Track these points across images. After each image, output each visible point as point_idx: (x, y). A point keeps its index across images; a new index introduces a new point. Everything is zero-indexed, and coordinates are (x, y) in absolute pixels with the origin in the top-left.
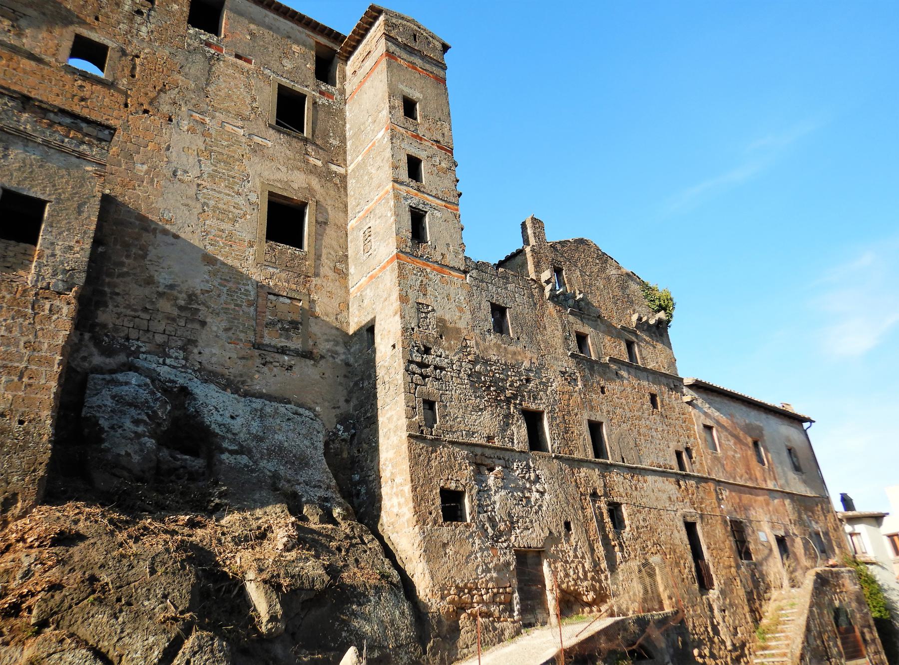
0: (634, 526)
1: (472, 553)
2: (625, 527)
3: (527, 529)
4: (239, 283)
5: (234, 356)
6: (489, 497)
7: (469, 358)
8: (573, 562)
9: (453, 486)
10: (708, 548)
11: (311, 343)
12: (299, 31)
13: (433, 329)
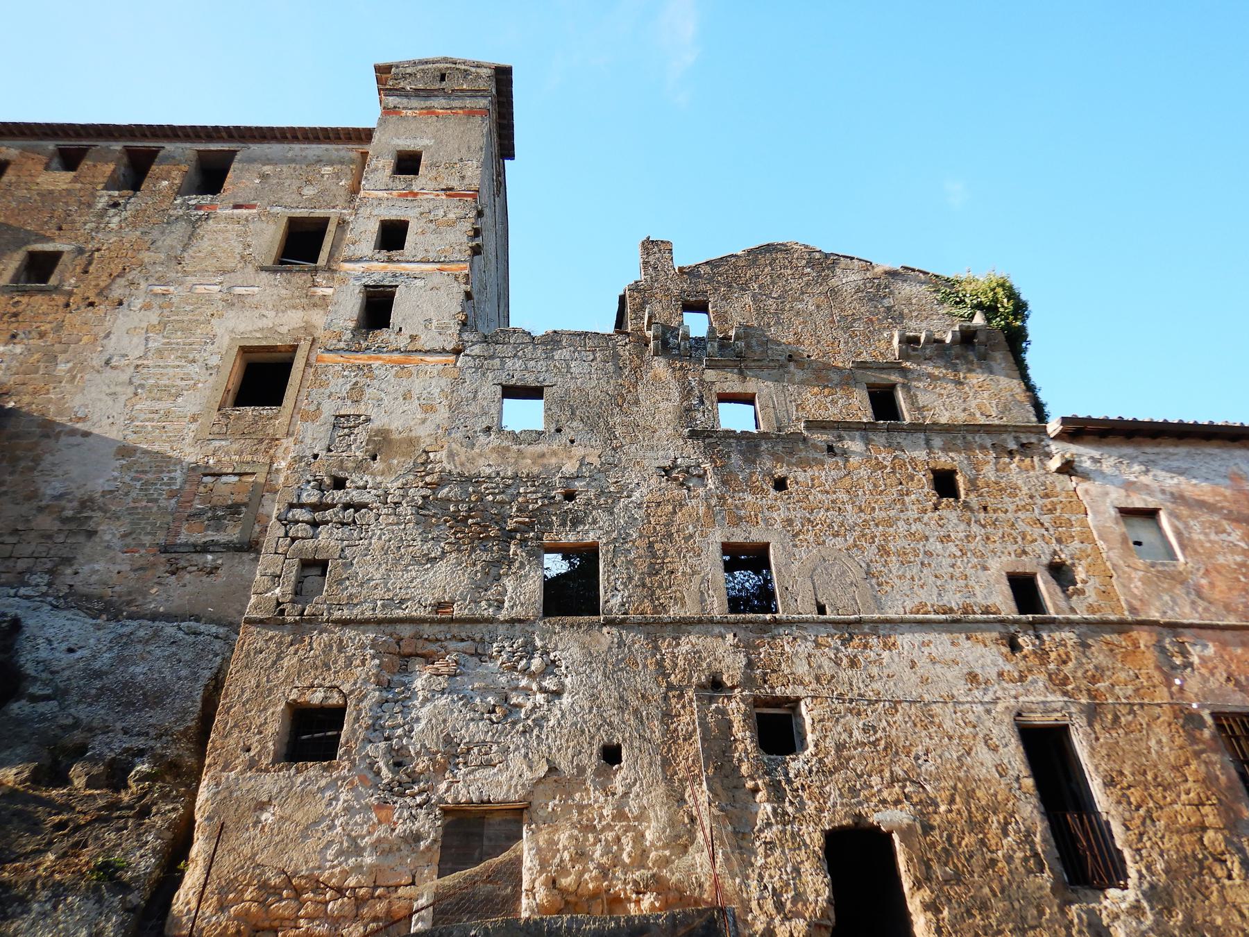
0: (829, 743)
1: (323, 818)
2: (804, 747)
3: (489, 764)
4: (162, 472)
5: (125, 568)
6: (405, 710)
7: (428, 479)
8: (609, 827)
9: (317, 697)
10: (1109, 783)
11: (257, 528)
12: (337, 150)
13: (358, 448)
